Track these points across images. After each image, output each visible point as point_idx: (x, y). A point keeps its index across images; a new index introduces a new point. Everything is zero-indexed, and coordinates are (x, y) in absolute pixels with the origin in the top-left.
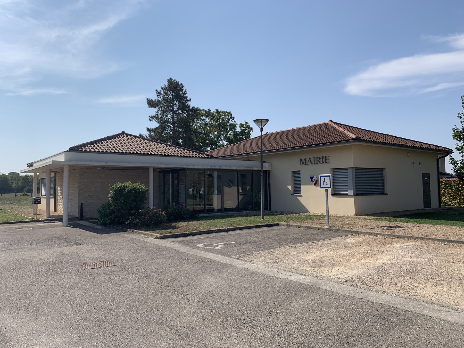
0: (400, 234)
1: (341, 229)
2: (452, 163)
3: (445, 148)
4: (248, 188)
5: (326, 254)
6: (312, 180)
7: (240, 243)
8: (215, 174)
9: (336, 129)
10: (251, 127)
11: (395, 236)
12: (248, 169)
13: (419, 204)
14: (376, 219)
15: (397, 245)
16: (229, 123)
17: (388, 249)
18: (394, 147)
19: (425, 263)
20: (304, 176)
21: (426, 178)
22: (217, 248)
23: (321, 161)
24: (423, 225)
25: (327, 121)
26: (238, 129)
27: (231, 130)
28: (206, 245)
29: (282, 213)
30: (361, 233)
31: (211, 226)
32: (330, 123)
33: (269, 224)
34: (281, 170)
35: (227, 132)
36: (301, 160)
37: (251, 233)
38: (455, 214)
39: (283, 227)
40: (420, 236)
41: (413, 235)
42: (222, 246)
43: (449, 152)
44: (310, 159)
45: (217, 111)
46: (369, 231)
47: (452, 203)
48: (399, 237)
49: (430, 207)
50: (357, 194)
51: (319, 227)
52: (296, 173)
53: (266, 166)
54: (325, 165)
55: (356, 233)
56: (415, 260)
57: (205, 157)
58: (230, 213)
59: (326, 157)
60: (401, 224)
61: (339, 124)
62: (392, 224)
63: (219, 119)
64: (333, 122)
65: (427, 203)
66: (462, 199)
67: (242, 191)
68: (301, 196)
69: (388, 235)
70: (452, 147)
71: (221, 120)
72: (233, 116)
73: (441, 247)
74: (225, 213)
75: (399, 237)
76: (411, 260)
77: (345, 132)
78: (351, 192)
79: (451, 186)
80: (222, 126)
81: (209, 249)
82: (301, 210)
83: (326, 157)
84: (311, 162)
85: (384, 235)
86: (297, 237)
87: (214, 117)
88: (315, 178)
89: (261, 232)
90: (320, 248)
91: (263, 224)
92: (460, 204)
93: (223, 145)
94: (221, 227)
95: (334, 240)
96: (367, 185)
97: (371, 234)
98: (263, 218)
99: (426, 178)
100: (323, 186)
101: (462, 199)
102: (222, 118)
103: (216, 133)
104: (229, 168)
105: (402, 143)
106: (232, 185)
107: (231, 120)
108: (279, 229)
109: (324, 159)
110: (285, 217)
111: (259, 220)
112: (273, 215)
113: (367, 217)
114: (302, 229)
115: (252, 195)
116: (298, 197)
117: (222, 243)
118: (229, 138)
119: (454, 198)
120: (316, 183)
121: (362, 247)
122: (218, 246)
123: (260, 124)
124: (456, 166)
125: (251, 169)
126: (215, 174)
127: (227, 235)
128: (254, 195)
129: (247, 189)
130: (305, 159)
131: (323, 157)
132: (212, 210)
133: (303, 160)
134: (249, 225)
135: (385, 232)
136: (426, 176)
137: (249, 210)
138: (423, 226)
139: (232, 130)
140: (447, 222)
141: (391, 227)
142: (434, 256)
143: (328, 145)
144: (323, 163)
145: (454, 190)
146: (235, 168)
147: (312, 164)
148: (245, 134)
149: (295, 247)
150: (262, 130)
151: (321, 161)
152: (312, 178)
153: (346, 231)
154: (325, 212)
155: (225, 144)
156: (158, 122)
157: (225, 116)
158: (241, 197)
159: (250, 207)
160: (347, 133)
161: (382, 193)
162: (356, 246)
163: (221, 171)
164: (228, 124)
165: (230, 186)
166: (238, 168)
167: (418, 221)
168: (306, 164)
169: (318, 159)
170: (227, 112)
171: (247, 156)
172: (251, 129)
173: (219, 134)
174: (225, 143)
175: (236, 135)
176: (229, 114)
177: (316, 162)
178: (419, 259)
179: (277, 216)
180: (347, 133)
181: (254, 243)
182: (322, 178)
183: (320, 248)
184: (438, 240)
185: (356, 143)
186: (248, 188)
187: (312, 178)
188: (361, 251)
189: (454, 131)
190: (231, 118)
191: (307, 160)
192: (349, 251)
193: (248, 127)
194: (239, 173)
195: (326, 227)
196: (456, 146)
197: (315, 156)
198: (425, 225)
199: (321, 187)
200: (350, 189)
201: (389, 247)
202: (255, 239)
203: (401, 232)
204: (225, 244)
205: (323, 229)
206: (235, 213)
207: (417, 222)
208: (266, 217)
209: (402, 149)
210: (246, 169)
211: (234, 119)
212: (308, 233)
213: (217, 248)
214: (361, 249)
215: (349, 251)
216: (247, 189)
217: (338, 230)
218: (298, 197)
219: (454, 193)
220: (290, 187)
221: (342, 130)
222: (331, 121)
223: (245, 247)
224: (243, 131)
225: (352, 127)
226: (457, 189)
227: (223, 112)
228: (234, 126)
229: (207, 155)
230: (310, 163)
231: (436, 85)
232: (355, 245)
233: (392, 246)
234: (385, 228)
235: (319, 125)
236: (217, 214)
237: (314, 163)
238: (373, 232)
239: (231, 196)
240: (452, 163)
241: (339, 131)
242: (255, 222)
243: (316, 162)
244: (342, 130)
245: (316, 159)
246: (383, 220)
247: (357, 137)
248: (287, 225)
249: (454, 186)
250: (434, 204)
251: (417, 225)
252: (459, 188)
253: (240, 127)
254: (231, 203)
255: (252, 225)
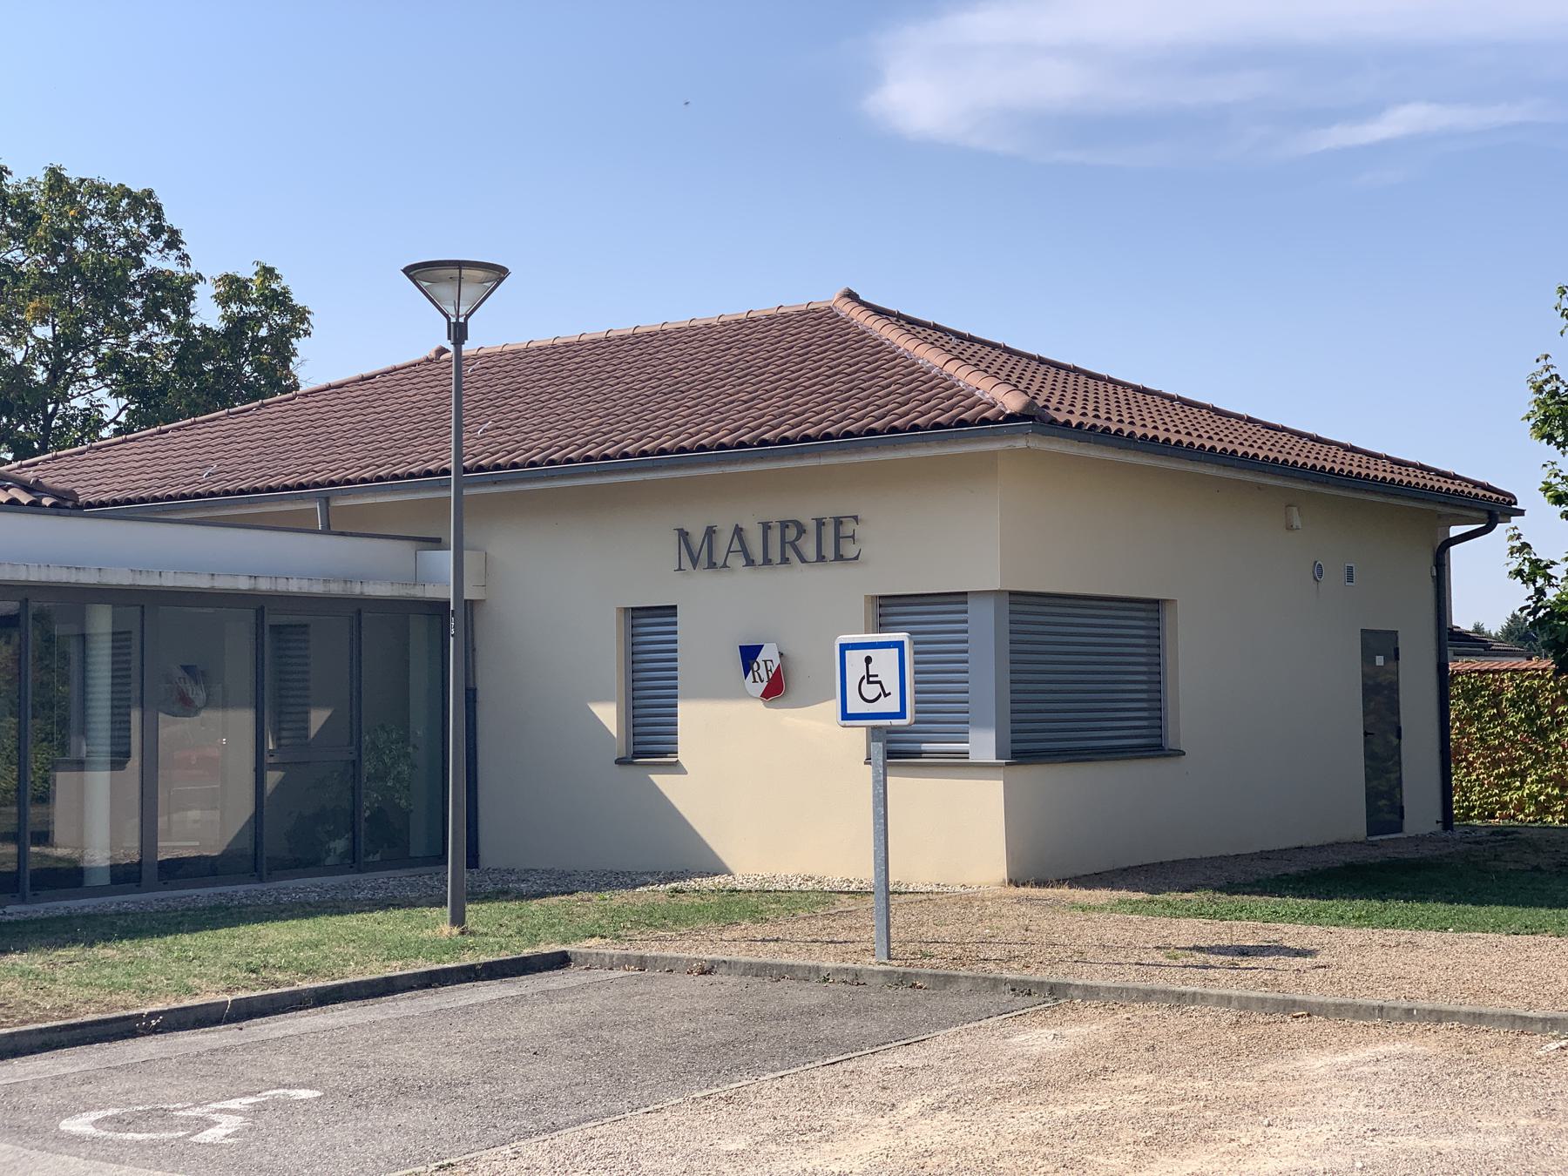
0: (1315, 997)
1: (963, 972)
2: (1519, 573)
3: (1476, 485)
4: (318, 718)
5: (932, 1132)
6: (747, 668)
7: (357, 1098)
8: (101, 622)
9: (894, 355)
10: (298, 300)
11: (1289, 1007)
12: (336, 589)
13: (1343, 817)
14: (1135, 908)
15: (1317, 1063)
16: (139, 264)
17: (1274, 1086)
18: (1189, 467)
19: (1508, 1160)
20: (702, 641)
21: (1380, 660)
22: (208, 1136)
23: (809, 547)
24: (1406, 935)
25: (823, 293)
26: (207, 313)
27: (153, 313)
28: (119, 1123)
29: (562, 883)
30: (1090, 992)
31: (114, 988)
32: (847, 309)
33: (505, 955)
34: (554, 595)
35: (123, 331)
36: (683, 535)
37: (405, 1026)
38: (1537, 869)
39: (604, 975)
40: (1426, 1004)
41: (1386, 997)
42: (235, 1122)
43: (1492, 508)
44: (738, 531)
45: (56, 178)
46: (1133, 979)
47: (1504, 806)
48: (1312, 1011)
49: (1400, 830)
50: (1021, 752)
51: (830, 963)
52: (649, 623)
53: (437, 575)
54: (833, 573)
55: (1056, 991)
56: (1446, 1143)
57: (13, 502)
58: (203, 895)
59: (838, 522)
60: (1290, 933)
61: (899, 316)
62: (1244, 932)
63: (67, 236)
64: (868, 306)
65: (1384, 806)
66: (1557, 780)
67: (277, 739)
68: (676, 768)
69: (1245, 1004)
70: (1525, 486)
71: (80, 244)
72: (170, 219)
73: (1547, 1061)
74: (160, 893)
75: (1312, 1011)
76: (1424, 1144)
77: (951, 368)
78: (983, 744)
79: (1497, 705)
80: (87, 287)
81: (153, 1145)
82: (672, 859)
83: (838, 522)
84: (745, 551)
85: (1226, 1000)
86: (718, 1037)
87: (32, 220)
88: (769, 654)
89: (467, 1010)
90: (884, 1097)
91: (468, 959)
92: (1544, 809)
93: (91, 422)
94: (189, 991)
95: (944, 1042)
96: (1072, 695)
97: (1147, 996)
98: (458, 919)
99: (1380, 660)
100: (856, 705)
101: (1557, 780)
102: (89, 234)
103: (44, 332)
104: (203, 582)
105: (1264, 450)
106: (198, 694)
107: (155, 245)
108: (583, 988)
109: (829, 532)
110: (588, 905)
111: (428, 933)
112: (502, 894)
113: (1080, 895)
114: (728, 982)
115: (356, 764)
116: (652, 777)
117: (233, 1104)
118: (141, 374)
119: (1513, 774)
120: (775, 689)
121: (1119, 1080)
122: (211, 1124)
123: (445, 292)
124: (1540, 592)
125: (357, 589)
126: (101, 622)
127: (246, 1048)
128: (368, 767)
129: (313, 731)
130: (710, 532)
131: (820, 523)
132: (70, 877)
133: (697, 537)
134: (377, 970)
135: (1225, 981)
136: (1380, 644)
137: (332, 871)
138: (1416, 946)
139: (163, 319)
140: (1525, 915)
141: (1244, 952)
142: (1537, 1114)
143: (860, 448)
144: (821, 558)
145: (1511, 726)
146: (243, 584)
147: (750, 562)
148: (256, 350)
149: (728, 1100)
150: (459, 333)
151: (809, 547)
152: (749, 654)
153: (996, 983)
154: (863, 872)
155: (109, 413)
156: (476, 358)
157: (111, 214)
158: (273, 778)
159: (340, 845)
160: (966, 377)
161: (1155, 747)
162: (1091, 1076)
163: (141, 605)
164: (134, 275)
165: (186, 706)
166: (264, 585)
167: (1369, 916)
168: (712, 565)
169: (792, 533)
170: (127, 193)
171: (317, 502)
172: (301, 315)
173: (70, 341)
174: (113, 407)
175: (193, 348)
176: (143, 203)
177: (775, 555)
178: (1468, 1141)
179: (535, 905)
180: (966, 377)
181: (445, 1089)
182: (855, 659)
183: (884, 1097)
184: (1522, 1024)
185: (1021, 444)
186: (318, 718)
187: (749, 654)
188: (1131, 1104)
189: (1539, 390)
190: (156, 231)
191: (724, 540)
192: (1060, 1112)
193: (279, 300)
194: (271, 619)
195: (870, 963)
196: (1544, 475)
197: (776, 514)
198: (1421, 937)
199: (846, 716)
200: (982, 725)
201: (1278, 1077)
202: (453, 1065)
203: (1315, 988)
204: (258, 1110)
205: (856, 978)
206: (240, 891)
207: (1362, 920)
208: (475, 913)
209: (1260, 487)
210: (318, 588)
211: (174, 242)
212: (773, 1006)
213: (208, 1136)
214: (1126, 1094)
215: (1060, 1112)
216: (313, 731)
217: (949, 980)
218: (652, 777)
219: (1513, 743)
220: (608, 715)
221: (930, 357)
222: (851, 296)
223: (403, 1118)
224: (238, 326)
225: (972, 340)
226: (1530, 719)
227: (97, 191)
228: (176, 292)
229: (26, 488)
230: (737, 561)
231: (1371, 110)
232: (1086, 1070)
233: (1288, 1068)
234: (1212, 959)
235: (782, 322)
236: (111, 903)
237: (767, 561)
238: (1160, 984)
239: (210, 773)
240: (1519, 573)
241: (912, 367)
242: (401, 949)
243: (775, 555)
244: (930, 357)
245: (775, 536)
246: (1173, 911)
247: (1031, 404)
248: (625, 961)
249: (1513, 703)
250: (1421, 814)
251: (1378, 935)
252: (1540, 715)
253: (223, 300)
254: (202, 822)
255: (395, 969)
